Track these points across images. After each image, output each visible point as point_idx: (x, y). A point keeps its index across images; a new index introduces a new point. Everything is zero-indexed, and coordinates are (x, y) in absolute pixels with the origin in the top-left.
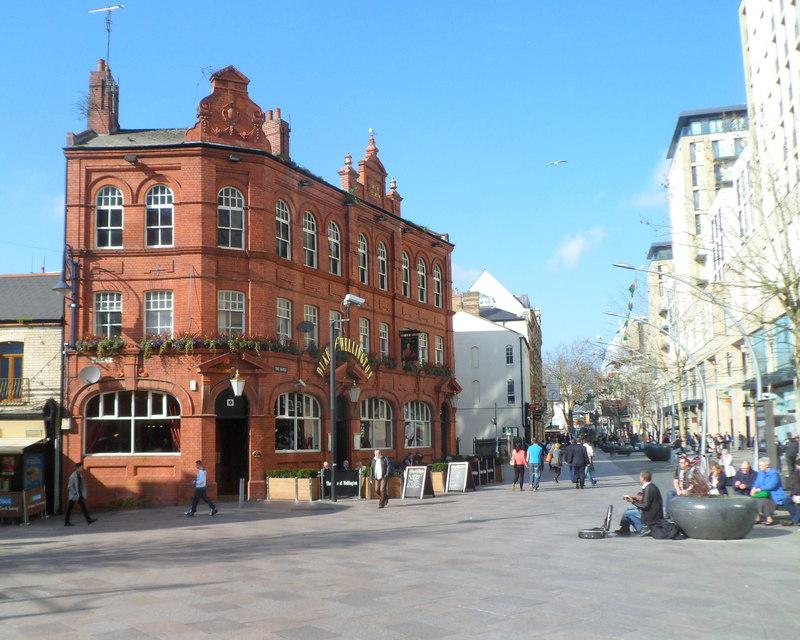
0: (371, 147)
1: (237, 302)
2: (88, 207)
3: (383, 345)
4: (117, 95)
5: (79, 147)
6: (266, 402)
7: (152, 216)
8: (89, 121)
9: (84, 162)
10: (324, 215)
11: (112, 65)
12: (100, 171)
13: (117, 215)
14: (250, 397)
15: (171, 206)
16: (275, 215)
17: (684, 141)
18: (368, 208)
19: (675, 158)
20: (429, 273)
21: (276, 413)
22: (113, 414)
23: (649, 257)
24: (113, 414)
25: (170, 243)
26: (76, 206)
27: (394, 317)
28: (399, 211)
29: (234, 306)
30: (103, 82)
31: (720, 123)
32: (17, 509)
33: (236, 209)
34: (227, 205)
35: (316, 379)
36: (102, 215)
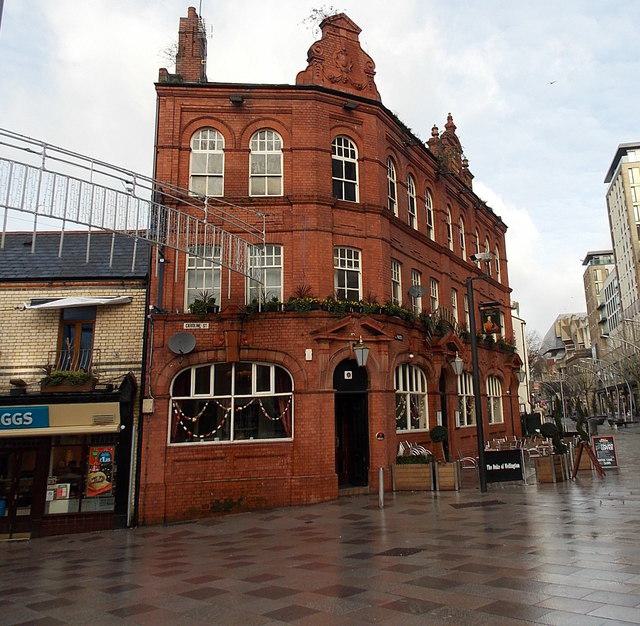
1: (353, 260)
5: (166, 85)
12: (196, 111)
15: (355, 161)
29: (350, 264)
32: (489, 467)
33: (349, 160)
34: (340, 154)
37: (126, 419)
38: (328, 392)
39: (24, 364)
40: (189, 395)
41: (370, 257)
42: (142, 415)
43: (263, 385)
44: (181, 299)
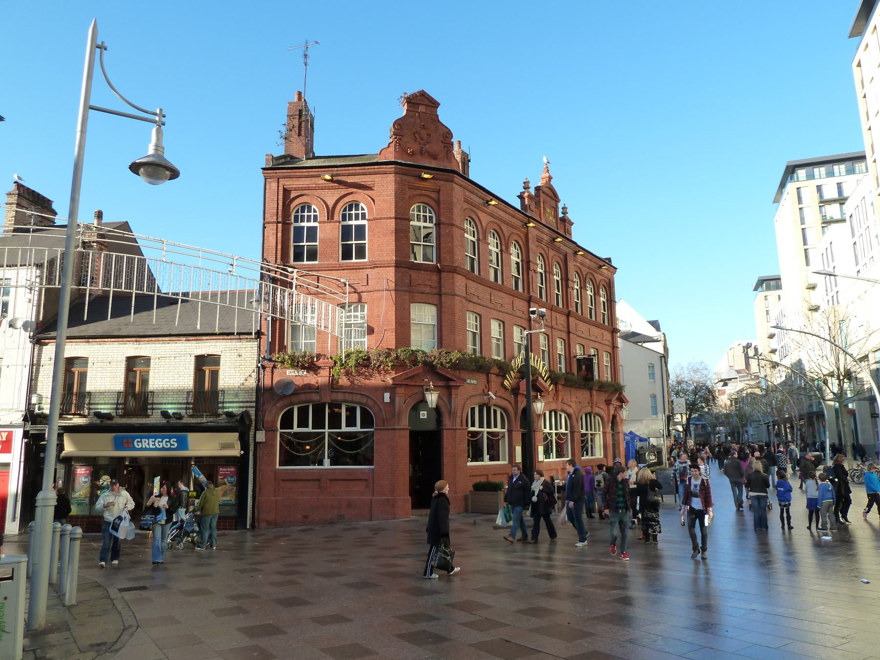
0: (547, 174)
2: (286, 224)
3: (560, 358)
4: (312, 126)
6: (459, 414)
7: (346, 232)
8: (286, 147)
9: (282, 182)
10: (507, 234)
11: (307, 97)
13: (312, 231)
14: (444, 409)
16: (465, 232)
17: (791, 187)
18: (546, 230)
19: (783, 201)
20: (596, 293)
21: (467, 426)
22: (307, 426)
23: (756, 289)
24: (307, 426)
25: (364, 258)
26: (273, 223)
27: (569, 333)
28: (571, 234)
30: (300, 111)
31: (823, 170)
34: (419, 220)
35: (503, 390)
36: (299, 231)
37: (245, 446)
38: (403, 429)
39: (170, 401)
40: (292, 429)
41: (179, 462)
42: (256, 444)
43: (351, 422)
44: (370, 233)
